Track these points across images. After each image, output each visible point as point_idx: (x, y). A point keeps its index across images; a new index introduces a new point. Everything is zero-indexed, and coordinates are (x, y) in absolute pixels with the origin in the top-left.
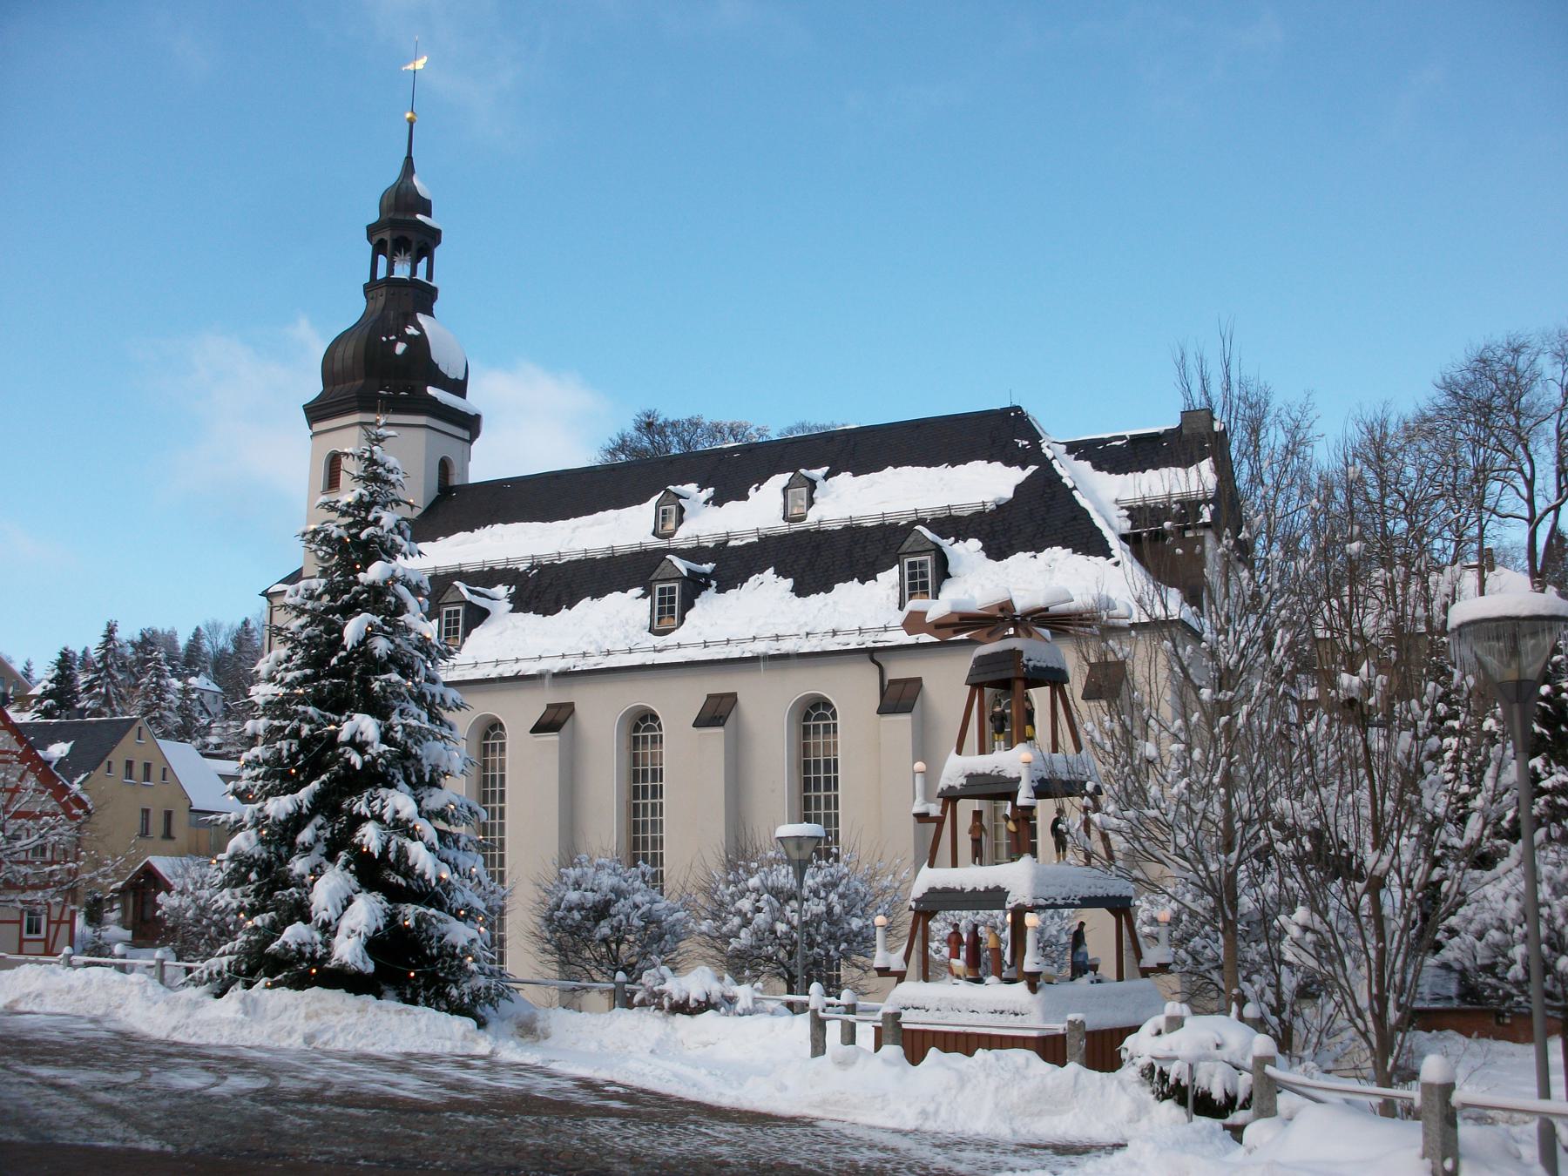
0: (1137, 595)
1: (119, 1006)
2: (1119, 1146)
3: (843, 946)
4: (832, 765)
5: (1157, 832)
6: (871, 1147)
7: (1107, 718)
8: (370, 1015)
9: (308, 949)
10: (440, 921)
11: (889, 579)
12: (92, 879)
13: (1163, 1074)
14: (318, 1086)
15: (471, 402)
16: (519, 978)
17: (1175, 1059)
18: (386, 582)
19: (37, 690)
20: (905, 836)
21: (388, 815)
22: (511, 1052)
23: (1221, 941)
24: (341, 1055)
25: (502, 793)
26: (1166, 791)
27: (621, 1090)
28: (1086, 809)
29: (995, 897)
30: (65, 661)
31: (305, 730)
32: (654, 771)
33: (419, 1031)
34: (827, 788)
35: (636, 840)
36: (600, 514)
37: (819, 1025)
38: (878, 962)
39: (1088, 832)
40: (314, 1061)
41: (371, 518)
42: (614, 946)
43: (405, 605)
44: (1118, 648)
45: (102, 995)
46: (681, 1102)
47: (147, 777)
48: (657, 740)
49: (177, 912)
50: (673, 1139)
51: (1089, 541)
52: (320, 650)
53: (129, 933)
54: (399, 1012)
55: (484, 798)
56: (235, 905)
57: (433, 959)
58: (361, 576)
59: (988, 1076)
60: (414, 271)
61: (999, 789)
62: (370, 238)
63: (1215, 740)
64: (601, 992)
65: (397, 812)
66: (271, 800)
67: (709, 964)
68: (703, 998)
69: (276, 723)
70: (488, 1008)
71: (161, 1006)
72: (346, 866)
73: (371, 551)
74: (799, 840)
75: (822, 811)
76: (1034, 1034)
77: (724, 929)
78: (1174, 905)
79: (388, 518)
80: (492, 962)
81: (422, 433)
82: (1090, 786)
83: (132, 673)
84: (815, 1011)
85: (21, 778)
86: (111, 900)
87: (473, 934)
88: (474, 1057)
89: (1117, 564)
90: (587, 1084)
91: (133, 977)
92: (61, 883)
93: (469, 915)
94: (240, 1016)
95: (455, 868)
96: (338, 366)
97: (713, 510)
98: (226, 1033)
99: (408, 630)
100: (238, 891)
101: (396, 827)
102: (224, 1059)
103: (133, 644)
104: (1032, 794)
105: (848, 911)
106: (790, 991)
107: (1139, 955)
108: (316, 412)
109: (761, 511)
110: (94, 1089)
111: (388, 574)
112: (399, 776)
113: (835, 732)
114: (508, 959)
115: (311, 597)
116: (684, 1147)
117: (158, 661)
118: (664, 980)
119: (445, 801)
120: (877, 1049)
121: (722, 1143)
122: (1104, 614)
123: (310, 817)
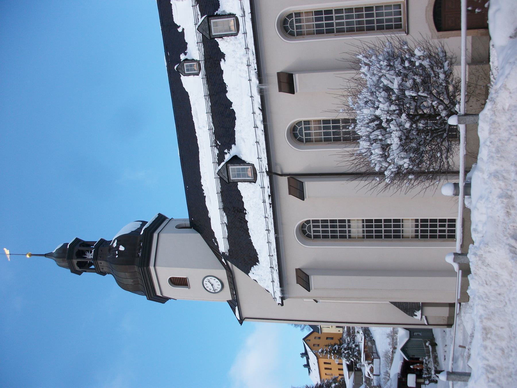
75: (321, 229)
96: (130, 281)
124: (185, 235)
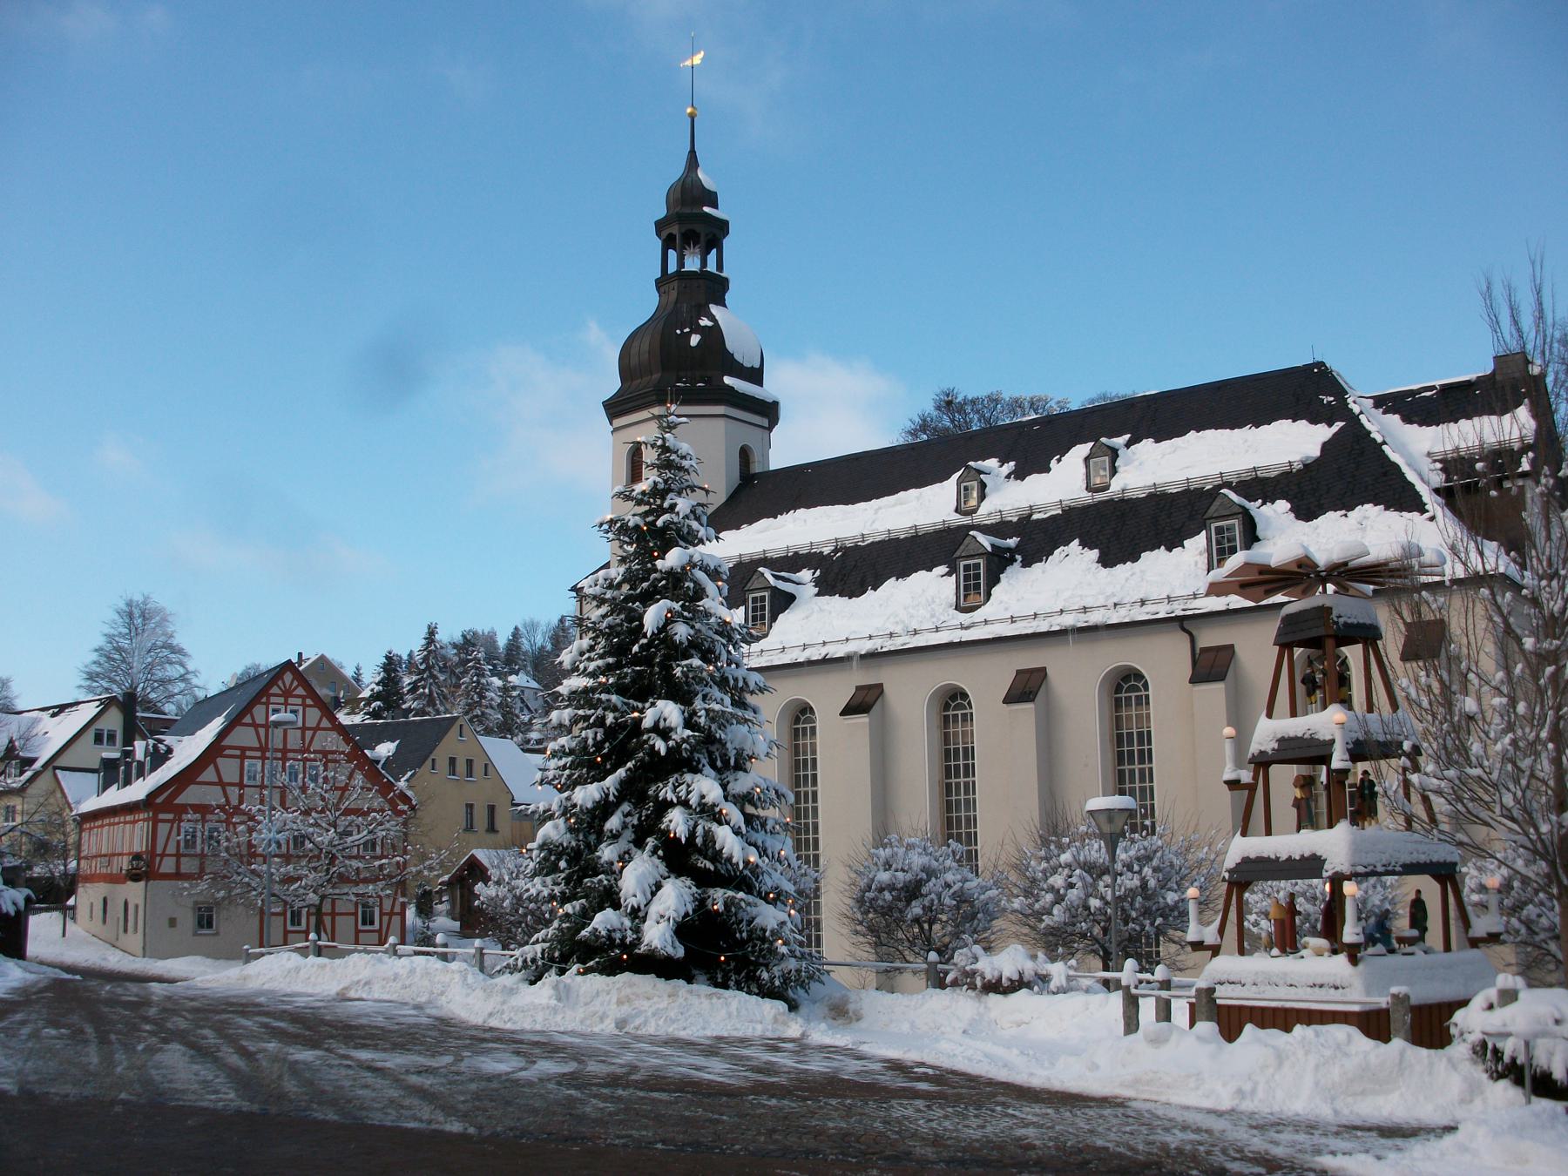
0: (1450, 542)
1: (442, 993)
2: (1450, 1129)
3: (1159, 921)
4: (1145, 738)
5: (1481, 793)
6: (1184, 1128)
7: (1423, 673)
8: (681, 1000)
9: (618, 935)
10: (749, 904)
11: (1197, 545)
12: (419, 872)
13: (1498, 1054)
14: (624, 1070)
15: (769, 389)
16: (830, 960)
17: (1509, 1035)
18: (683, 568)
19: (366, 694)
20: (1224, 804)
21: (693, 800)
22: (821, 1034)
23: (1557, 909)
24: (653, 1040)
25: (815, 777)
26: (1490, 748)
27: (930, 1071)
28: (1405, 769)
29: (1311, 865)
30: (391, 665)
31: (610, 718)
32: (966, 749)
33: (730, 1015)
34: (1142, 761)
35: (949, 820)
36: (902, 494)
37: (1132, 1003)
38: (1192, 934)
39: (1407, 796)
40: (625, 1046)
41: (666, 505)
42: (926, 926)
43: (703, 590)
44: (1433, 605)
45: (426, 983)
46: (991, 1083)
47: (470, 774)
48: (968, 718)
49: (495, 901)
50: (979, 1122)
51: (1402, 498)
52: (621, 641)
53: (458, 924)
54: (709, 996)
55: (797, 782)
56: (546, 893)
57: (743, 943)
58: (659, 563)
59: (1307, 1053)
60: (704, 263)
61: (1313, 752)
62: (658, 234)
63: (1541, 692)
64: (915, 973)
65: (703, 797)
66: (578, 789)
67: (1023, 943)
68: (1015, 977)
69: (581, 712)
70: (801, 991)
71: (479, 993)
72: (654, 852)
73: (666, 538)
74: (1109, 813)
75: (1137, 785)
76: (1356, 1008)
77: (1037, 906)
78: (1504, 871)
79: (683, 504)
80: (801, 944)
81: (721, 422)
82: (1407, 746)
83: (453, 673)
84: (1128, 987)
85: (350, 777)
86: (440, 893)
87: (783, 917)
88: (784, 1040)
89: (1432, 519)
90: (896, 1066)
91: (454, 965)
92: (391, 877)
93: (778, 898)
94: (553, 1002)
95: (763, 851)
96: (634, 361)
97: (1015, 485)
98: (540, 1018)
99: (708, 615)
100: (549, 879)
101: (702, 811)
102: (536, 1044)
103: (455, 646)
104: (1347, 757)
105: (1163, 885)
106: (1106, 968)
107: (1466, 923)
108: (615, 408)
109: (1064, 482)
110: (407, 1072)
111: (685, 560)
112: (704, 761)
113: (1148, 703)
114: (824, 941)
115: (610, 586)
116: (989, 1129)
117: (478, 661)
118: (976, 959)
119: (750, 784)
120: (1192, 1025)
121: (1031, 1126)
122: (1414, 561)
123: (617, 805)
124: (723, 471)
